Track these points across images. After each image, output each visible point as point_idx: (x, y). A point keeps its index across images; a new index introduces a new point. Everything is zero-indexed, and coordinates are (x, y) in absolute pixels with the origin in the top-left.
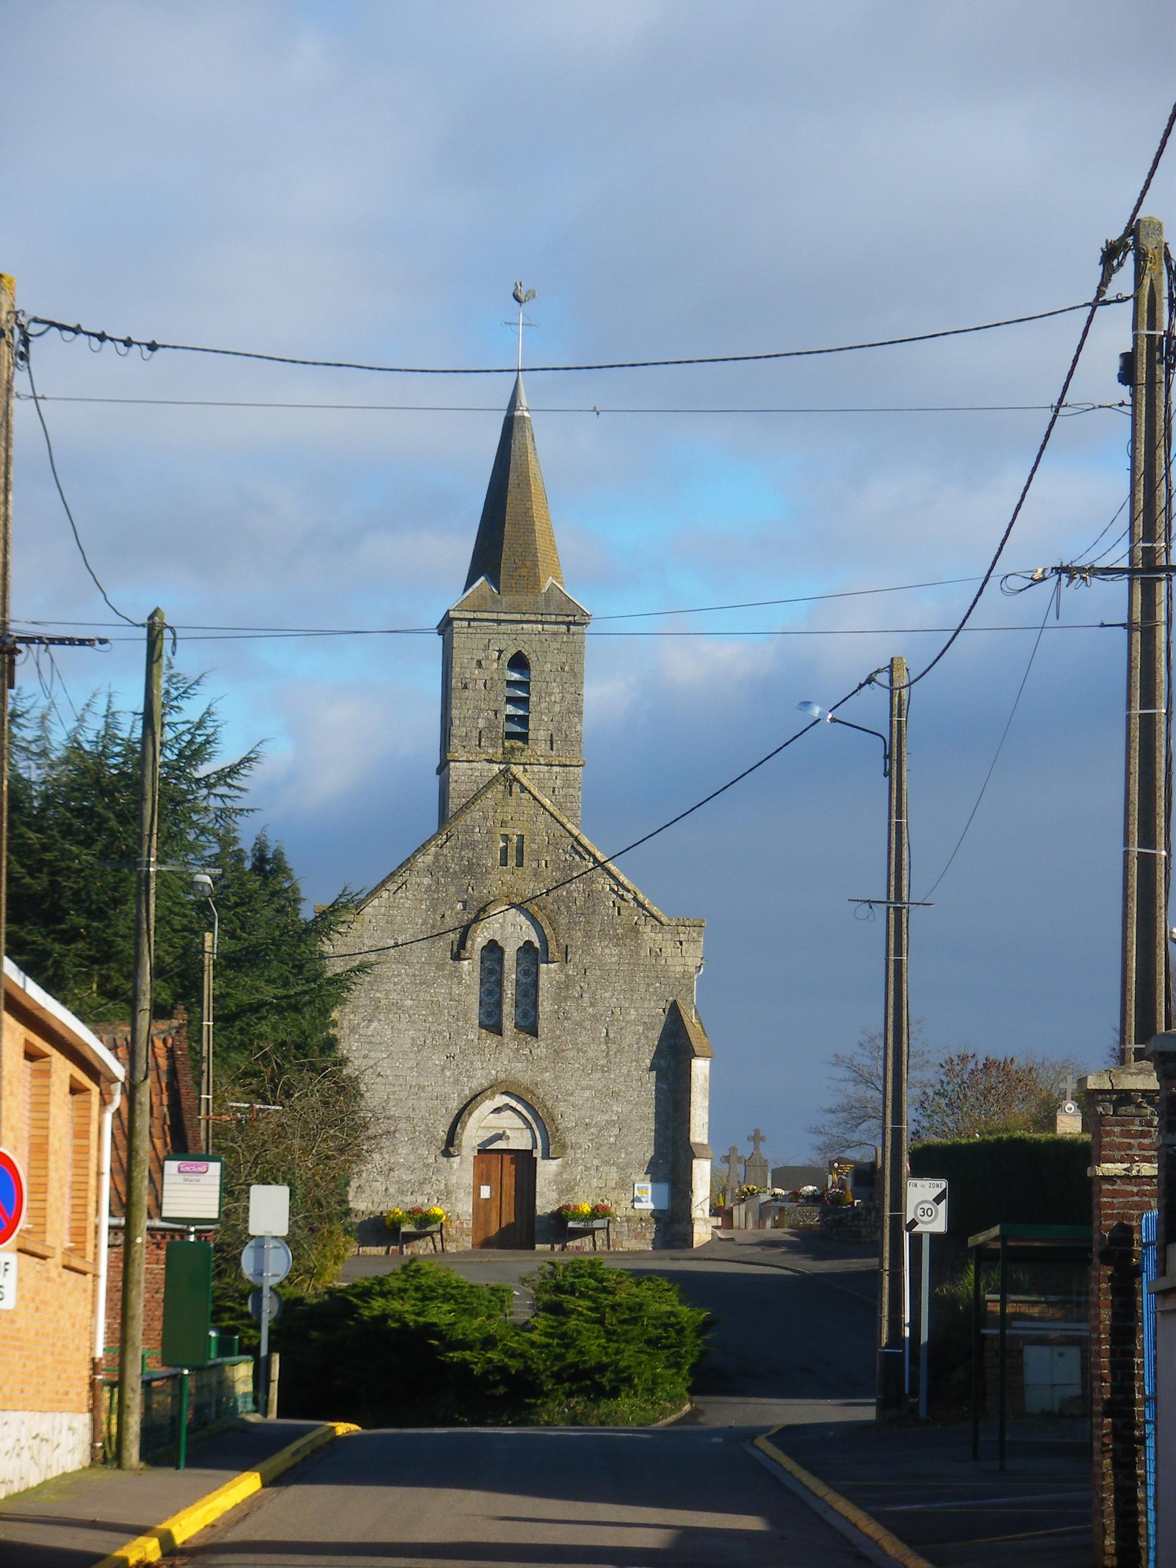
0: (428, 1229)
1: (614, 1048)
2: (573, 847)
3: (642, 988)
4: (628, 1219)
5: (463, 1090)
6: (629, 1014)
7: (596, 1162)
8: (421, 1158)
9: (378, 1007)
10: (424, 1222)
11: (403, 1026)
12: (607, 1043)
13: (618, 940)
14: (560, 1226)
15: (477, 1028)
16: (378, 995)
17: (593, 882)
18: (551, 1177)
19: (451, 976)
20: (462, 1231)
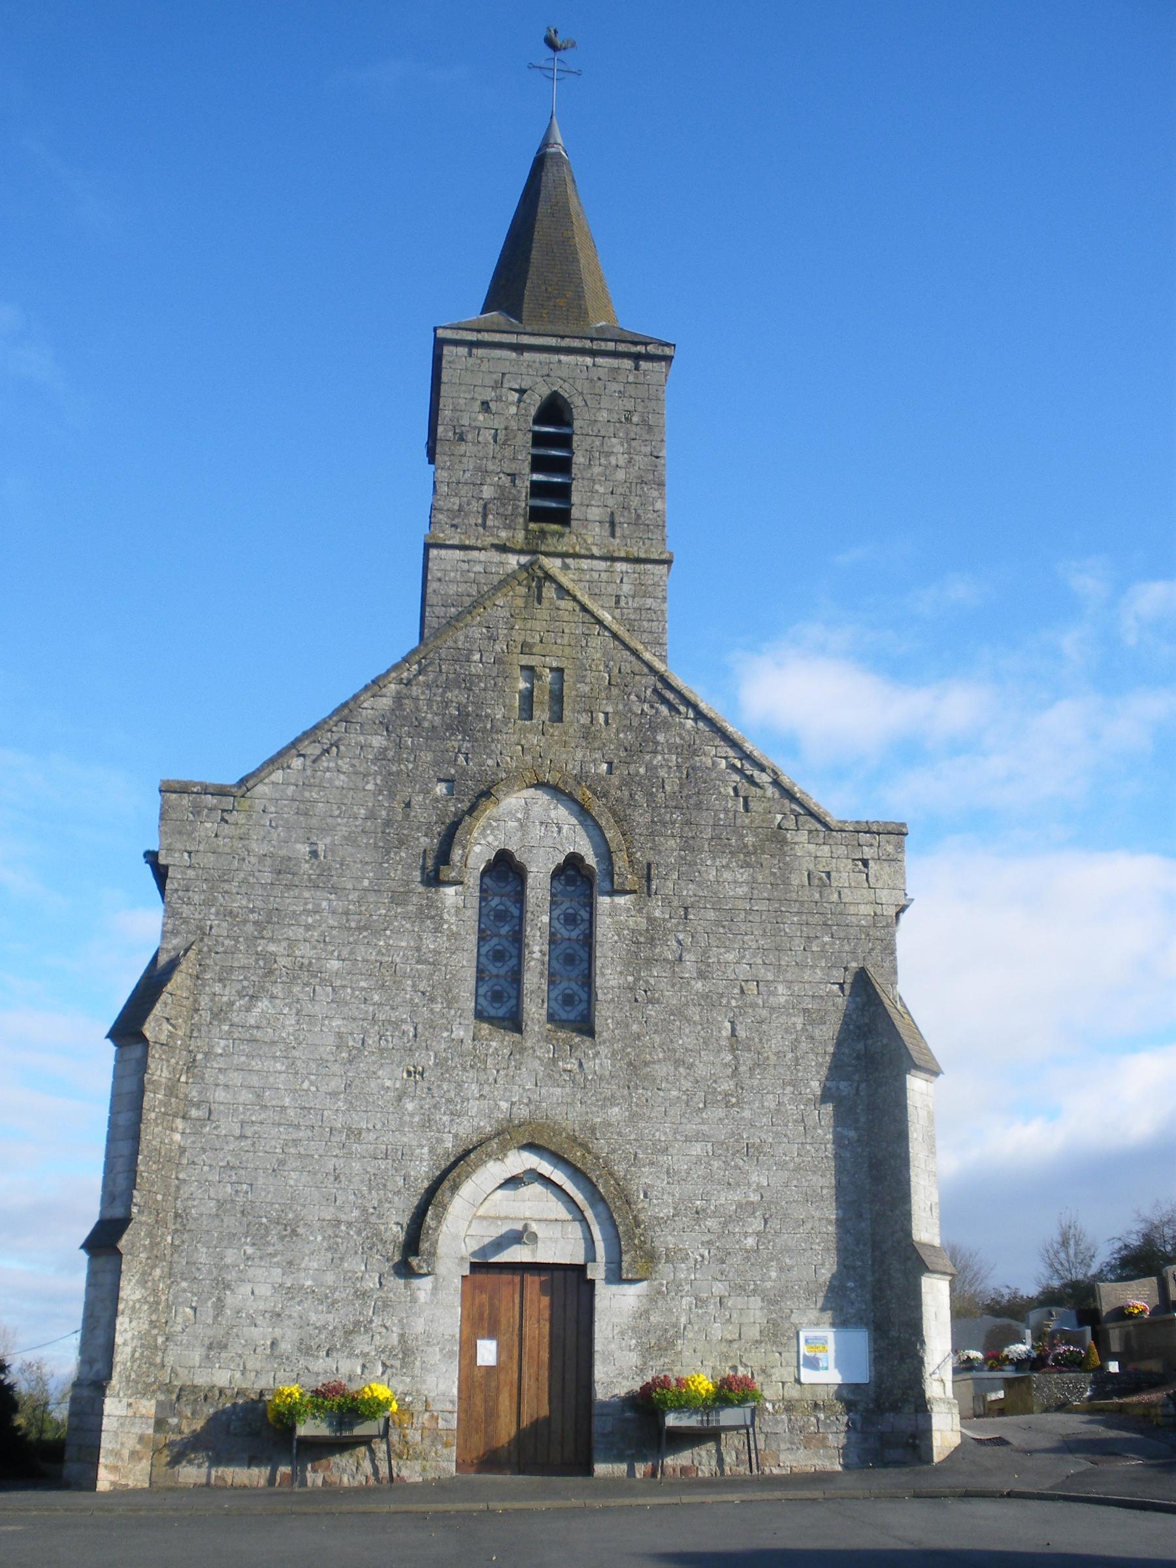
0: (360, 1430)
1: (747, 1058)
2: (655, 691)
3: (798, 944)
4: (790, 1407)
5: (440, 1141)
6: (774, 993)
7: (719, 1288)
8: (350, 1278)
9: (271, 972)
10: (349, 1413)
11: (318, 1009)
12: (733, 1050)
13: (747, 857)
14: (648, 1421)
15: (470, 1019)
16: (272, 948)
17: (695, 753)
18: (624, 1320)
19: (421, 915)
20: (435, 1436)
